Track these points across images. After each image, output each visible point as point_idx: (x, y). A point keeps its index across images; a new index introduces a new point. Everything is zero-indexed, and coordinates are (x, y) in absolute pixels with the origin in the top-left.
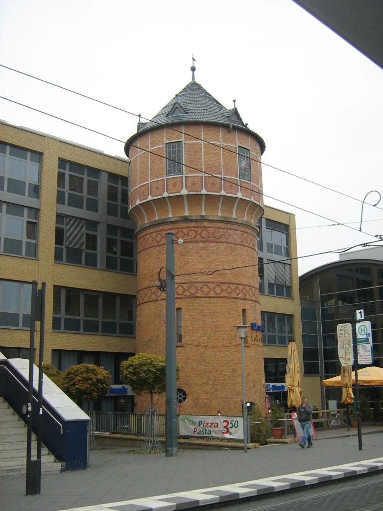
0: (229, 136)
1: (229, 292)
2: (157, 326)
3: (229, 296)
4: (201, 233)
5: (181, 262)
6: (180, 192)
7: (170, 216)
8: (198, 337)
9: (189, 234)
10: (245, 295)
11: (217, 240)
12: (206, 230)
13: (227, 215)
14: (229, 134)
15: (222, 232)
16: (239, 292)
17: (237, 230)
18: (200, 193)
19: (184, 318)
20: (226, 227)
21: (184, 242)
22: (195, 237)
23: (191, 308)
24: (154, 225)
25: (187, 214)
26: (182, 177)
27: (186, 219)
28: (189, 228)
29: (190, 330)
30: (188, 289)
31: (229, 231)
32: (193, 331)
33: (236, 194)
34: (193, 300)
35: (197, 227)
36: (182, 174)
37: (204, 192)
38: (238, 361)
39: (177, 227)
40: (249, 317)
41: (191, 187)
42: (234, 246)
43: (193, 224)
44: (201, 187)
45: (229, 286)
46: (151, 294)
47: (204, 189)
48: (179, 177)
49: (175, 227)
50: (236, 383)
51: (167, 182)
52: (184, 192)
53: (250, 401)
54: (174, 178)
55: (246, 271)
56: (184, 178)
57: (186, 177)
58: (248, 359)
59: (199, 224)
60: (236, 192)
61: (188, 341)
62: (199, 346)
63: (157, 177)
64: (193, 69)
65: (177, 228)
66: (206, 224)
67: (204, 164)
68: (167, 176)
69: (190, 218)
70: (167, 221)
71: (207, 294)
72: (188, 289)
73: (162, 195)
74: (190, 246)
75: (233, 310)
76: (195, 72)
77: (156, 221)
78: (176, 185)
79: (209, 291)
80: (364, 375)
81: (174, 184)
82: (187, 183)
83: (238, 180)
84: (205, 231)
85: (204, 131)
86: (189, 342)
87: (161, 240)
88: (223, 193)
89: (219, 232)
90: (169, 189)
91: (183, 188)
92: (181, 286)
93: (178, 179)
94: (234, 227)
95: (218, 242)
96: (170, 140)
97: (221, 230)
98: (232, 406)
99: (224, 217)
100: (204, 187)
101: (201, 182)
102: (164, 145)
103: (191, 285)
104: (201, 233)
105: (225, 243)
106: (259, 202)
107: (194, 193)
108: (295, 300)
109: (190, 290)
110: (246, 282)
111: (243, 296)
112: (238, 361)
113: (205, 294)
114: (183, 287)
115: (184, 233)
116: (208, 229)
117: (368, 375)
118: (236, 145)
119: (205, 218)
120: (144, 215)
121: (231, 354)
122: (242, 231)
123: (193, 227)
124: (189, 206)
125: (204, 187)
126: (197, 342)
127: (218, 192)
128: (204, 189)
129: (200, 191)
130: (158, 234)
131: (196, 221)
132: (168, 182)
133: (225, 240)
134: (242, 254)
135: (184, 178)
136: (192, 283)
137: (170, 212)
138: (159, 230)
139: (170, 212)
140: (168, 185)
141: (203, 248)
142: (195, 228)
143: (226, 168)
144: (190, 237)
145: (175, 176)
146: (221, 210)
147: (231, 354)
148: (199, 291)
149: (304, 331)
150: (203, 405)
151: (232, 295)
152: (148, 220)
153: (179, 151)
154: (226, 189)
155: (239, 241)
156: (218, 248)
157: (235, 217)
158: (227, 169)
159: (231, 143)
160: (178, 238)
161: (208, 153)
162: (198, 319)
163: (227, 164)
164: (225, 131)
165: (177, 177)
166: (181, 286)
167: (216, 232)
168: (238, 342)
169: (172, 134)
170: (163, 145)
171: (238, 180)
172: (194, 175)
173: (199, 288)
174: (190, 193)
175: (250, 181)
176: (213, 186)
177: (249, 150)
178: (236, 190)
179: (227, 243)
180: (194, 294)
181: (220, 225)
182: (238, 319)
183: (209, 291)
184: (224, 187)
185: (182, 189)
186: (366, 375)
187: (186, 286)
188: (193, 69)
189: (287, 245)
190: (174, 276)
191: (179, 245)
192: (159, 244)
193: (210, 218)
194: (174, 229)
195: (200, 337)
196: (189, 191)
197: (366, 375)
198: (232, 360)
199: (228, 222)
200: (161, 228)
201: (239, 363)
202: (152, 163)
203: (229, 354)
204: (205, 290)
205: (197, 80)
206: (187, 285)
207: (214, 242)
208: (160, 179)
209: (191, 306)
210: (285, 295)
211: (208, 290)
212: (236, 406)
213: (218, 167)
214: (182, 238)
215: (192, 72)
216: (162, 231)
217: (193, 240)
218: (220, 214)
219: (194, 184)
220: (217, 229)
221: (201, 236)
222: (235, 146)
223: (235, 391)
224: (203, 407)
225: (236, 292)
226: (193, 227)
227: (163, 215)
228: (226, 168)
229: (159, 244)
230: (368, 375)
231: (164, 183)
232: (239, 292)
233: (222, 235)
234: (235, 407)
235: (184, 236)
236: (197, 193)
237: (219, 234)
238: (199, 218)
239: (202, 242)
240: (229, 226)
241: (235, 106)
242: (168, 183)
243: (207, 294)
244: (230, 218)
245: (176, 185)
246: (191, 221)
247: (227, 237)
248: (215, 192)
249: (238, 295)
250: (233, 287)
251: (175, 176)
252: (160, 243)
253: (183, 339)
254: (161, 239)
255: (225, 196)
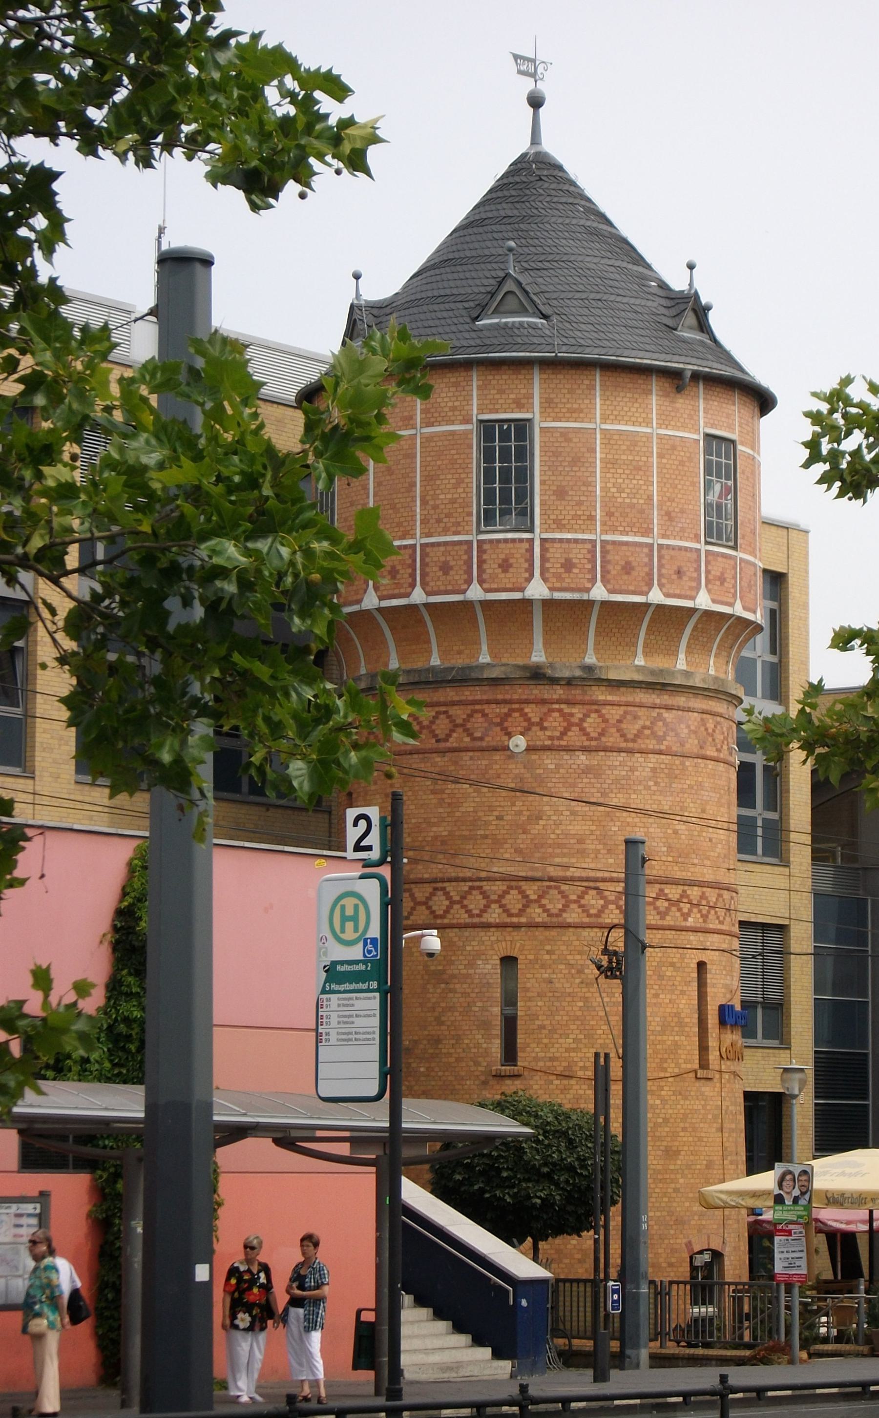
0: (681, 403)
1: (662, 909)
2: (433, 1009)
3: (660, 922)
4: (582, 720)
5: (520, 813)
6: (522, 590)
7: (485, 658)
8: (568, 1050)
9: (545, 724)
10: (705, 917)
11: (630, 745)
12: (597, 711)
13: (659, 662)
14: (678, 396)
15: (644, 717)
16: (690, 911)
17: (689, 710)
18: (585, 597)
19: (527, 990)
20: (658, 701)
21: (529, 749)
22: (564, 733)
23: (547, 957)
24: (428, 683)
25: (538, 656)
26: (531, 541)
27: (536, 675)
28: (543, 702)
29: (542, 1027)
30: (540, 897)
31: (666, 714)
32: (553, 1031)
33: (693, 598)
34: (554, 933)
35: (568, 702)
36: (531, 530)
37: (599, 593)
38: (682, 1125)
39: (508, 697)
40: (714, 986)
41: (559, 577)
42: (677, 761)
43: (559, 692)
44: (589, 576)
45: (661, 890)
46: (412, 904)
47: (599, 583)
48: (521, 540)
49: (500, 697)
50: (676, 1190)
51: (481, 551)
52: (537, 590)
53: (713, 1247)
54: (506, 541)
55: (711, 840)
56: (537, 543)
57: (543, 541)
58: (710, 1116)
59: (576, 693)
60: (691, 588)
61: (536, 1059)
62: (570, 1077)
63: (446, 531)
64: (536, 102)
65: (505, 702)
66: (601, 695)
67: (601, 502)
68: (479, 532)
69: (549, 672)
70: (474, 675)
71: (598, 915)
72: (540, 897)
73: (464, 592)
74: (549, 761)
75: (672, 964)
76: (541, 110)
77: (433, 669)
78: (511, 566)
79: (604, 907)
80: (843, 1174)
81: (506, 560)
82: (548, 560)
83: (699, 550)
84: (593, 715)
85: (604, 399)
86: (541, 1064)
87: (449, 736)
88: (656, 596)
89: (636, 717)
90: (485, 576)
91: (532, 575)
92: (518, 888)
93: (517, 545)
94: (681, 700)
95: (630, 752)
96: (491, 411)
97: (641, 712)
98: (661, 1260)
99: (652, 672)
100: (599, 576)
101: (589, 561)
102: (472, 427)
103: (549, 887)
104: (582, 720)
105: (654, 752)
106: (755, 612)
107: (568, 596)
108: (795, 868)
109: (544, 901)
110: (709, 875)
111: (700, 924)
112: (682, 1125)
113: (589, 916)
114: (522, 892)
115: (528, 720)
116: (605, 710)
117: (856, 1174)
118: (697, 431)
119: (598, 674)
120: (384, 642)
121: (664, 1101)
122: (703, 712)
123: (558, 702)
124: (546, 632)
125: (599, 576)
126: (565, 1064)
127: (641, 593)
128: (599, 583)
129: (588, 590)
130: (438, 713)
131: (570, 682)
132: (485, 552)
133: (652, 744)
134: (700, 785)
135: (537, 543)
136: (551, 879)
137: (485, 648)
138: (442, 699)
139: (485, 648)
140: (484, 561)
141: (587, 770)
142: (563, 706)
143: (668, 513)
144: (548, 733)
145: (510, 536)
146: (646, 645)
147: (664, 1101)
148: (573, 906)
149: (818, 988)
150: (579, 1256)
151: (669, 921)
152: (402, 658)
153: (523, 454)
154: (664, 581)
155: (692, 745)
156: (632, 769)
157: (684, 667)
158: (668, 516)
159: (684, 428)
160: (510, 735)
161: (614, 463)
162: (569, 994)
163: (671, 500)
164: (667, 385)
165: (513, 541)
166: (518, 888)
167: (628, 717)
168: (683, 1066)
169: (501, 392)
170: (469, 427)
171: (698, 551)
172: (569, 536)
173: (574, 897)
174: (558, 595)
175: (735, 548)
176: (628, 573)
177: (733, 442)
178: (694, 584)
179: (660, 753)
180: (557, 915)
181: (642, 697)
182: (683, 993)
183: (604, 907)
184: (660, 576)
185: (529, 580)
186: (850, 1175)
187: (532, 889)
188: (536, 102)
189: (773, 651)
190: (644, 947)
191: (513, 756)
192: (442, 745)
193: (612, 676)
194: (497, 702)
195: (574, 1050)
196: (551, 589)
197: (850, 1175)
198: (666, 1121)
199: (664, 685)
200: (451, 694)
201: (684, 1129)
202: (428, 479)
203: (658, 1102)
204: (593, 902)
205: (551, 146)
206: (535, 886)
207: (620, 751)
208: (456, 538)
209: (548, 952)
210: (760, 850)
211: (602, 902)
212: (673, 1260)
213: (642, 512)
214: (522, 734)
215: (531, 110)
216: (453, 704)
217: (556, 743)
218: (640, 661)
219: (568, 566)
220: (630, 708)
221: (582, 729)
222: (695, 437)
223: (671, 1213)
224: (580, 1261)
225: (680, 910)
226: (558, 702)
227: (460, 652)
228: (668, 513)
229: (442, 745)
230: (856, 1174)
231: (469, 552)
232: (690, 911)
233: (644, 727)
234: (671, 1265)
235: (528, 729)
236: (576, 596)
237: (637, 727)
238: (578, 673)
239: (585, 750)
240: (665, 699)
241: (691, 285)
242: (485, 557)
243: (598, 915)
244: (672, 673)
245: (511, 566)
246: (554, 681)
247: (661, 733)
248: (634, 593)
249: (685, 917)
250: (673, 892)
251: (510, 536)
252: (448, 745)
253: (520, 1054)
254: (452, 731)
255: (660, 607)
